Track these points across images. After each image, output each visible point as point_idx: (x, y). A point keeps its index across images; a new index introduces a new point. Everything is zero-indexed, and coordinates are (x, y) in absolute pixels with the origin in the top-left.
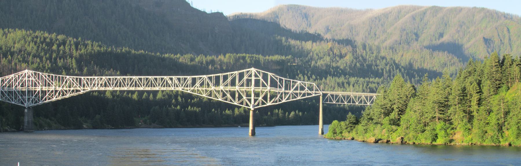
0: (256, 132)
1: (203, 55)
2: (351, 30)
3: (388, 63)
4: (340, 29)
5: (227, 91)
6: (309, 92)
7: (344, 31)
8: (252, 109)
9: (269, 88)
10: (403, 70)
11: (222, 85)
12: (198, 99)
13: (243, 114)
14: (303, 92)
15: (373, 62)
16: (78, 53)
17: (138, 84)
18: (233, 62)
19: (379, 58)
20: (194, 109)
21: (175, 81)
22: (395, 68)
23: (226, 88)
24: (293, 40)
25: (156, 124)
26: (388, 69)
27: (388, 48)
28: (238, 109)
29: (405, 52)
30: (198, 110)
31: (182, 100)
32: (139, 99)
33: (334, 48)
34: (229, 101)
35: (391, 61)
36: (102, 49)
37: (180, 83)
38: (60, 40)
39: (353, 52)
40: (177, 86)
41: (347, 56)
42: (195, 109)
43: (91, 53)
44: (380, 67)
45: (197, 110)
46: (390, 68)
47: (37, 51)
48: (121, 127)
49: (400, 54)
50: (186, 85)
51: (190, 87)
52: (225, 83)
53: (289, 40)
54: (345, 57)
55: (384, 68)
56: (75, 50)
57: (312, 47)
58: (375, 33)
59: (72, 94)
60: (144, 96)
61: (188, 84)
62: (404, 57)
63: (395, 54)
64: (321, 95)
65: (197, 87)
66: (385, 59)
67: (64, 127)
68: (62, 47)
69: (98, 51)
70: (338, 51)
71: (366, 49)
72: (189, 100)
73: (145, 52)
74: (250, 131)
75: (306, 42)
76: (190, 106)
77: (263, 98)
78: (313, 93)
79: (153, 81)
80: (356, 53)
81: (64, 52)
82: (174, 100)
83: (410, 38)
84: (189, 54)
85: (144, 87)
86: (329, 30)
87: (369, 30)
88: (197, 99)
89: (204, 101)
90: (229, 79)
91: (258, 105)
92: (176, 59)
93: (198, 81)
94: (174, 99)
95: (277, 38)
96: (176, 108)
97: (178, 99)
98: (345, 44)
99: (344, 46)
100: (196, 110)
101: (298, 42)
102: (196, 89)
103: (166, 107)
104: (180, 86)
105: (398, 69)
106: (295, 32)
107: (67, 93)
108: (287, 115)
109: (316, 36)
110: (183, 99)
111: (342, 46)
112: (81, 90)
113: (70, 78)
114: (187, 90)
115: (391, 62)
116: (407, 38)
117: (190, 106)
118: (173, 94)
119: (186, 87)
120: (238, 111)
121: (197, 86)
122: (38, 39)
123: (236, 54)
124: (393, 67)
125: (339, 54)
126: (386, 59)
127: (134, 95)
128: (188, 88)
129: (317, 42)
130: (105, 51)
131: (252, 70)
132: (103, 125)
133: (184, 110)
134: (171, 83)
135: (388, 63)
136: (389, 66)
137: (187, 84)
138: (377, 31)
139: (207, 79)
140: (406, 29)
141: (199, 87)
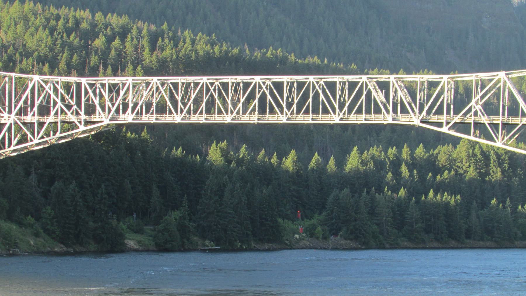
12: (453, 172)
16: (154, 56)
17: (270, 103)
21: (396, 92)
25: (341, 236)
30: (452, 202)
31: (411, 175)
32: (298, 171)
36: (217, 49)
38: (115, 27)
40: (404, 111)
42: (446, 199)
43: (188, 57)
45: (452, 200)
47: (51, 50)
48: (241, 246)
50: (435, 109)
51: (448, 113)
56: (147, 49)
59: (52, 139)
60: (312, 163)
61: (443, 102)
65: (472, 113)
67: (62, 246)
68: (117, 42)
69: (208, 53)
72: (430, 174)
73: (322, 61)
76: (432, 190)
79: (320, 92)
81: (120, 54)
82: (390, 175)
85: (289, 113)
88: (450, 171)
89: (467, 178)
94: (391, 172)
96: (395, 195)
97: (402, 173)
100: (449, 202)
102: (472, 122)
103: (368, 192)
107: (34, 137)
110: (415, 171)
112: (80, 122)
113: (46, 82)
114: (440, 125)
117: (432, 190)
118: (387, 160)
119: (435, 113)
121: (473, 110)
122: (61, 23)
127: (286, 158)
128: (443, 119)
130: (223, 54)
132: (188, 240)
133: (418, 202)
134: (384, 100)
137: (438, 104)
141: (479, 113)
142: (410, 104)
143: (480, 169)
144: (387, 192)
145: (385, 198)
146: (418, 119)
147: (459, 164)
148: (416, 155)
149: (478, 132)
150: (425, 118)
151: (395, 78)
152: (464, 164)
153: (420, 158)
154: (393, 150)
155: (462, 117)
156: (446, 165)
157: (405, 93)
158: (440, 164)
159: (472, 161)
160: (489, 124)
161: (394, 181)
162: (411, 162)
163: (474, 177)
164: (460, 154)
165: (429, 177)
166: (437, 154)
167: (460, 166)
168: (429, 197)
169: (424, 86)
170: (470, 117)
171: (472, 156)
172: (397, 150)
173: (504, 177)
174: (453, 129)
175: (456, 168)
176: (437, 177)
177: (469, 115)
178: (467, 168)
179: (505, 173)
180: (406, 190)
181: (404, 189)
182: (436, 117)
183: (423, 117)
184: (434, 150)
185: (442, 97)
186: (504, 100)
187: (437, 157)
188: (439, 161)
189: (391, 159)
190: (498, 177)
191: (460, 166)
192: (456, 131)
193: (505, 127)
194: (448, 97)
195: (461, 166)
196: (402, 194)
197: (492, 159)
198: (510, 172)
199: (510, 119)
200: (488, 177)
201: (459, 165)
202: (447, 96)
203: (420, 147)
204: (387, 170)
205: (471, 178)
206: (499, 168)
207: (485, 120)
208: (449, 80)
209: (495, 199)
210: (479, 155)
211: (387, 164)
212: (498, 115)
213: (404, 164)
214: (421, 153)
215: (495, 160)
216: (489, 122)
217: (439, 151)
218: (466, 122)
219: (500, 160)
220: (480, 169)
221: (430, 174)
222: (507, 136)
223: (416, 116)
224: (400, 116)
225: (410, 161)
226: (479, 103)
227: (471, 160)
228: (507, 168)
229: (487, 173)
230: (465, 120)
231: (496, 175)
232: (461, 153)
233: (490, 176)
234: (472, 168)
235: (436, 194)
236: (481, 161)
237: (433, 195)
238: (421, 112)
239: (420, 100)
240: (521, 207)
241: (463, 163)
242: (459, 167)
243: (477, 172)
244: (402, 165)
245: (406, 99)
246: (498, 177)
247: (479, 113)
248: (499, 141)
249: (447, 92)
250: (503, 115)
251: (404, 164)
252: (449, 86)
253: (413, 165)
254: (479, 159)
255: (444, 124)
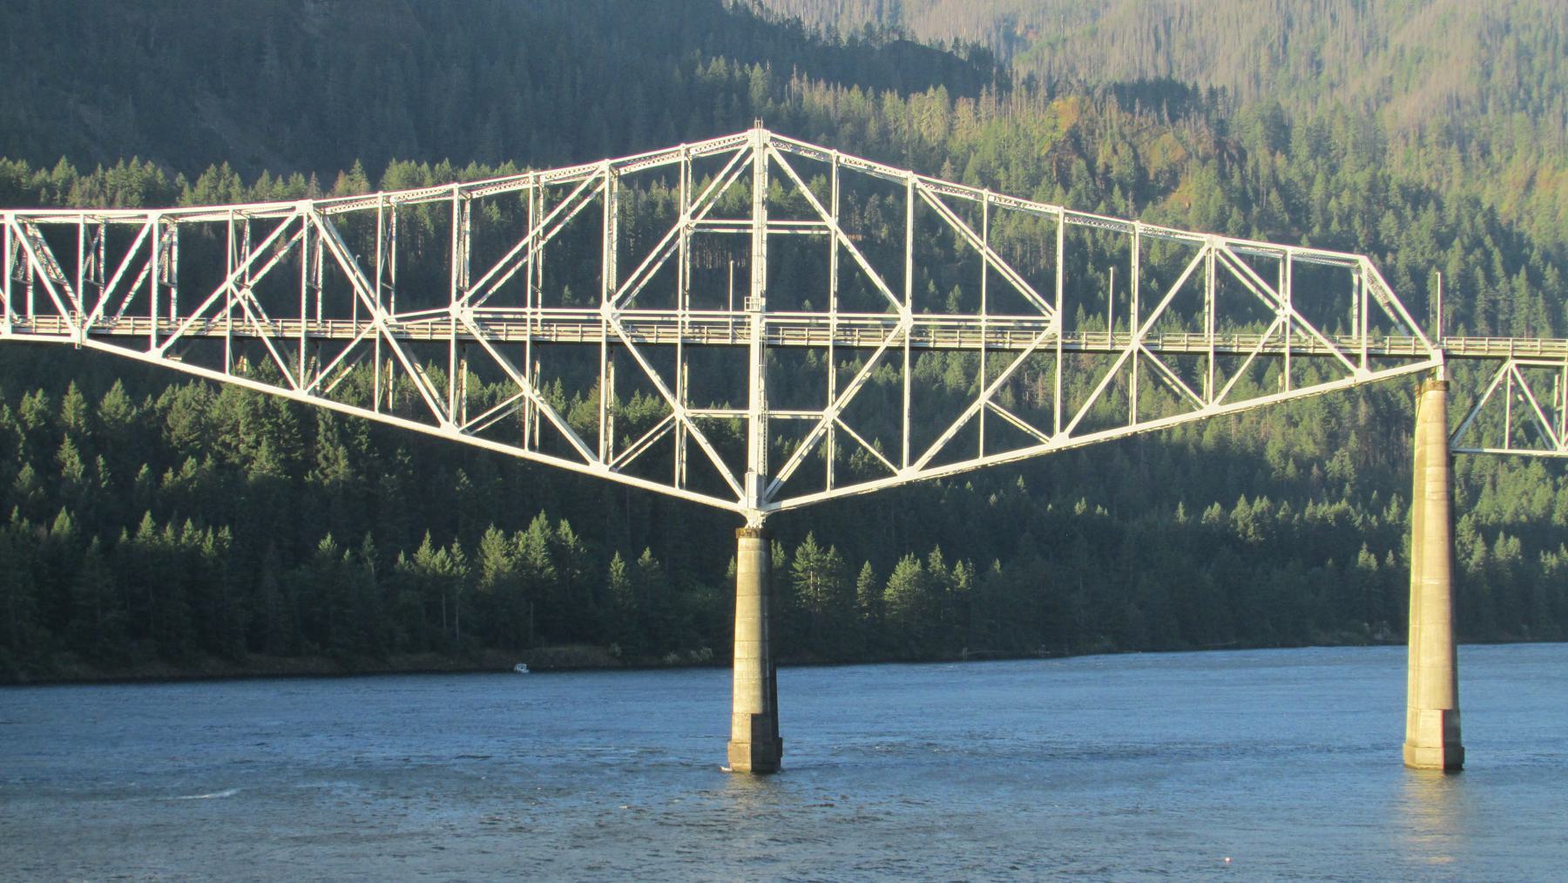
0: (783, 730)
1: (234, 170)
2: (1163, 37)
3: (1454, 232)
4: (1094, 34)
5: (513, 350)
6: (1317, 341)
7: (1118, 43)
8: (755, 519)
9: (905, 317)
10: (1551, 275)
11: (468, 295)
12: (209, 462)
13: (542, 569)
14: (1252, 344)
15: (1357, 222)
18: (433, 220)
19: (1395, 199)
20: (178, 533)
21: (21, 254)
22: (1503, 263)
23: (498, 320)
24: (822, 84)
26: (1453, 267)
27: (1431, 138)
28: (508, 536)
29: (1546, 157)
30: (208, 546)
31: (90, 470)
33: (1092, 133)
34: (532, 447)
35: (1472, 218)
37: (71, 273)
39: (1221, 161)
40: (45, 307)
41: (1181, 188)
42: (191, 538)
44: (1402, 256)
46: (1467, 264)
49: (1515, 173)
51: (164, 311)
52: (498, 274)
53: (794, 82)
54: (1166, 192)
55: (1431, 262)
57: (951, 128)
58: (1314, 54)
62: (1541, 192)
63: (1478, 178)
64: (1429, 373)
65: (228, 311)
66: (1432, 205)
70: (1124, 151)
71: (1293, 145)
72: (145, 469)
74: (741, 732)
75: (905, 96)
77: (844, 415)
78: (1355, 359)
80: (1241, 168)
82: (27, 472)
83: (1540, 84)
84: (135, 161)
86: (1018, 40)
87: (1274, 35)
89: (251, 478)
90: (532, 233)
91: (810, 476)
92: (44, 191)
93: (240, 257)
94: (31, 465)
95: (700, 69)
96: (43, 530)
97: (62, 465)
98: (1164, 107)
99: (1162, 122)
100: (199, 548)
101: (856, 95)
102: (227, 334)
104: (69, 305)
105: (1523, 272)
106: (823, 35)
108: (868, 586)
109: (961, 62)
110: (101, 460)
111: (1148, 119)
114: (141, 343)
115: (1473, 226)
116: (1520, 84)
117: (148, 515)
118: (18, 428)
119: (130, 312)
120: (508, 555)
121: (231, 303)
123: (453, 164)
124: (1488, 254)
125: (1129, 170)
126: (1440, 207)
128: (151, 326)
129: (984, 92)
131: (750, 151)
133: (108, 548)
135: (1454, 232)
136: (1464, 248)
137: (137, 286)
138: (1323, 39)
139: (323, 234)
140: (1513, 23)
141: (248, 312)
142: (59, 288)
143: (288, 451)
144: (17, 523)
145: (13, 539)
146: (82, 327)
147: (228, 438)
148: (103, 413)
149: (245, 361)
150: (100, 324)
151: (17, 217)
152: (242, 436)
153: (116, 421)
154: (37, 400)
155: (201, 323)
156: (192, 441)
157: (46, 256)
158: (173, 438)
159: (265, 429)
160: (271, 339)
161: (41, 490)
162: (89, 433)
163: (271, 474)
164: (229, 408)
165: (140, 476)
166: (166, 410)
167: (230, 444)
168: (140, 534)
169: (96, 239)
170: (221, 321)
171: (266, 415)
172: (47, 399)
173: (358, 474)
174: (178, 353)
175: (220, 448)
176: (166, 475)
177: (219, 316)
178: (250, 447)
179: (361, 462)
180: (73, 514)
181: (69, 513)
182: (131, 322)
183: (96, 323)
184: (155, 399)
185: (147, 267)
186: (312, 274)
187: (164, 418)
188: (170, 430)
189: (31, 426)
190: (341, 472)
191: (230, 444)
192: (185, 360)
193: (318, 347)
194: (161, 267)
195: (234, 444)
196: (62, 527)
197: (321, 423)
198: (375, 458)
199: (329, 325)
200: (310, 472)
201: (228, 441)
202: (160, 267)
203: (114, 388)
204: (20, 459)
205: (263, 476)
206: (341, 448)
207: (262, 329)
208: (164, 221)
209: (329, 537)
210: (284, 412)
211: (18, 439)
212: (296, 315)
213: (67, 441)
214: (118, 407)
215: (330, 422)
216: (272, 334)
217: (171, 401)
218: (212, 334)
219: (347, 425)
220: (288, 451)
221: (145, 469)
222: (322, 370)
223: (77, 320)
224: (34, 320)
225: (87, 431)
226: (247, 282)
227: (263, 425)
228: (364, 447)
229: (310, 463)
230: (209, 330)
231: (336, 467)
232: (233, 407)
233: (317, 472)
234: (264, 450)
235: (159, 527)
236: (290, 427)
237: (153, 528)
238: (89, 307)
239: (87, 275)
240: (406, 559)
241: (238, 435)
242: (227, 446)
243: (281, 461)
244: (62, 443)
245: (48, 274)
246: (341, 472)
247: (248, 312)
248: (299, 386)
249: (160, 254)
250: (311, 314)
251: (67, 441)
252: (166, 237)
253: (94, 440)
254: (285, 422)
255: (154, 341)
